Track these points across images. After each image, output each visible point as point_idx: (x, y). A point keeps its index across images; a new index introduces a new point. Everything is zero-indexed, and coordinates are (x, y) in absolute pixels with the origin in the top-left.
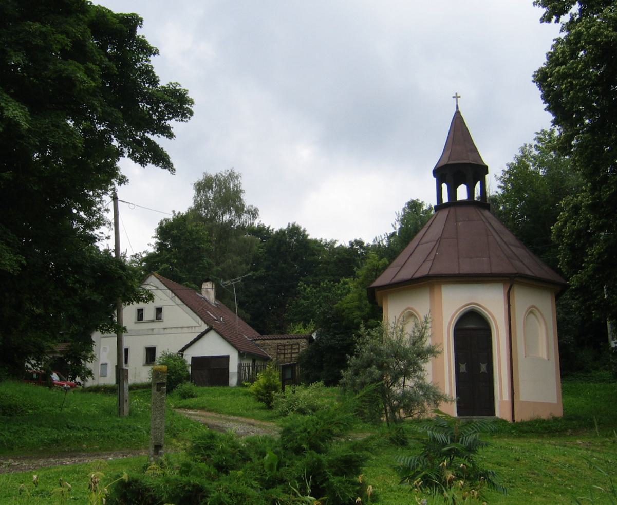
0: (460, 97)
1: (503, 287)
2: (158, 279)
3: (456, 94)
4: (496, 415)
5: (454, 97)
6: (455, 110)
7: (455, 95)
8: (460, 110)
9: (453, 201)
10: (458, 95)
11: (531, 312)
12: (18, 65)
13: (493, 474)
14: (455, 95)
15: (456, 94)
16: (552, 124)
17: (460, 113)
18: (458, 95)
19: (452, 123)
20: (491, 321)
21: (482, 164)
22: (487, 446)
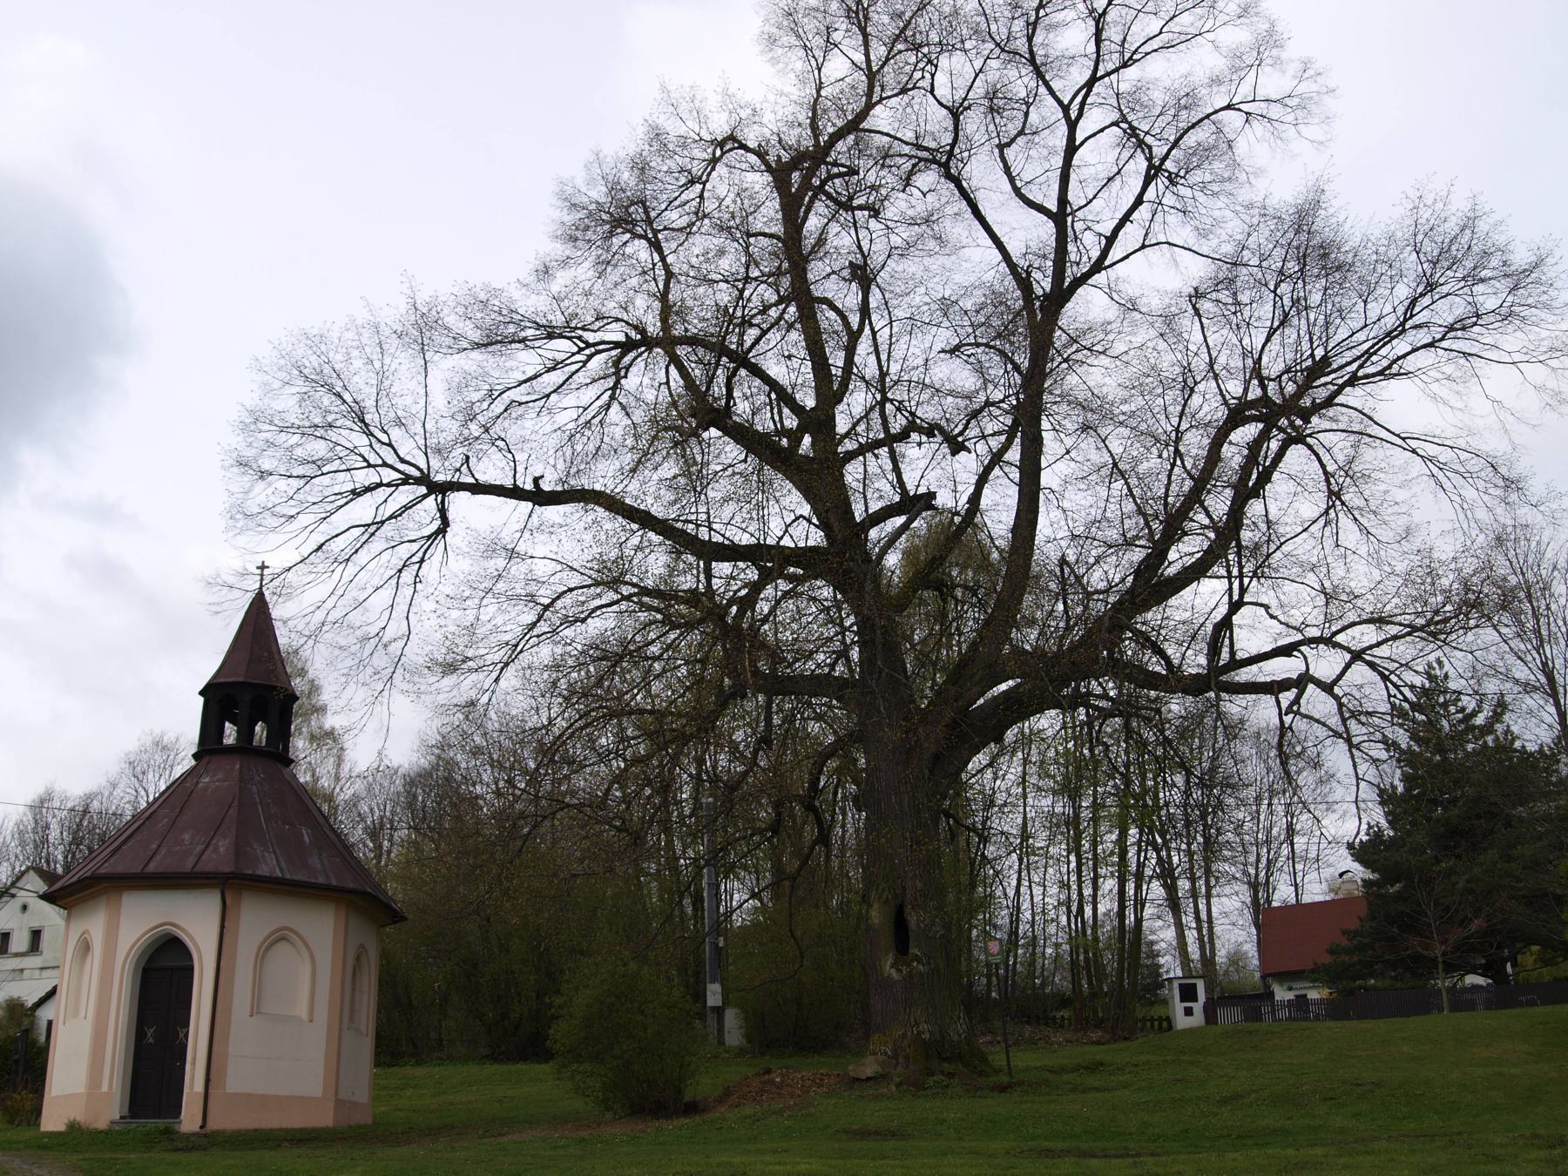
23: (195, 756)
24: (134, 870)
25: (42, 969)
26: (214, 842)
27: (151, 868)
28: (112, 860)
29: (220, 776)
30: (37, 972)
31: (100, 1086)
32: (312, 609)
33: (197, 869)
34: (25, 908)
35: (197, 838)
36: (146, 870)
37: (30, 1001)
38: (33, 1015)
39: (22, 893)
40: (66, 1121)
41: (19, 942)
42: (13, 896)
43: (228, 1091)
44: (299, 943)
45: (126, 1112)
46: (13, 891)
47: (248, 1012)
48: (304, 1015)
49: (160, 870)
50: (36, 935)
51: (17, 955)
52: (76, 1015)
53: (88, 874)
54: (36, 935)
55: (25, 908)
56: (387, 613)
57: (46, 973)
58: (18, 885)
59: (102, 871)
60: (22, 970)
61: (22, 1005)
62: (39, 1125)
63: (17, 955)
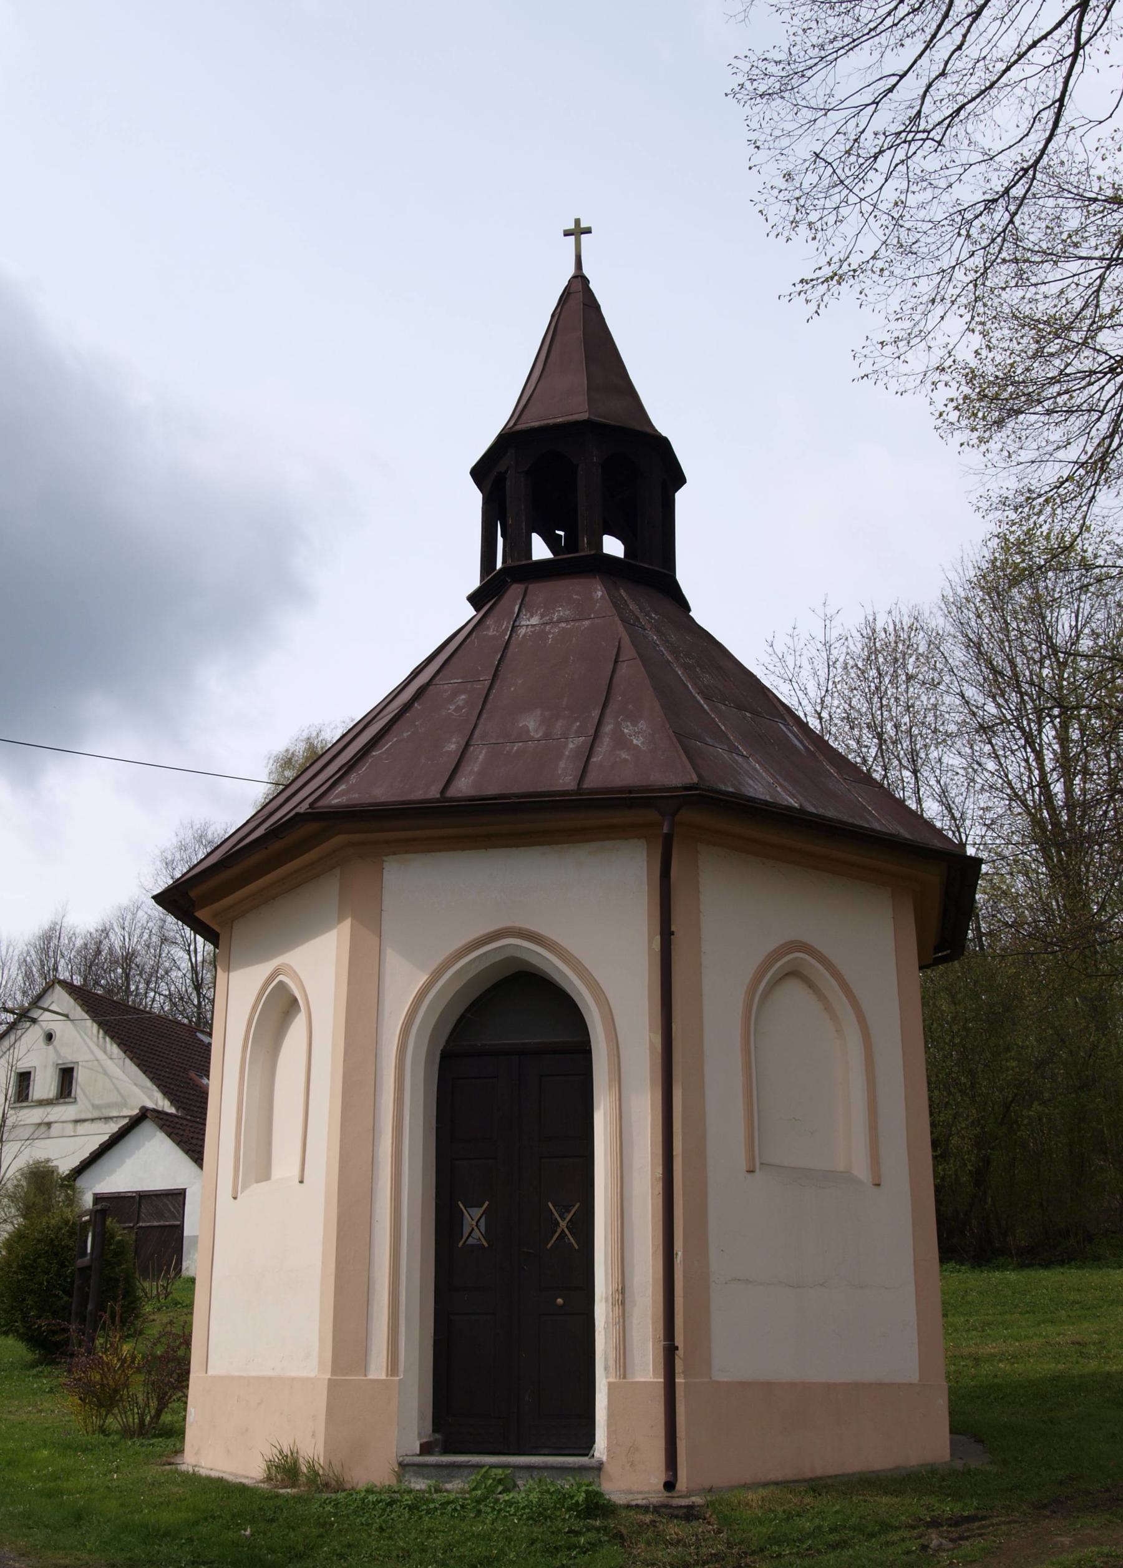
0: (588, 231)
1: (645, 857)
2: (836, 1476)
3: (577, 222)
4: (597, 1454)
5: (567, 233)
6: (571, 271)
7: (572, 226)
8: (587, 271)
9: (524, 562)
10: (583, 225)
11: (793, 973)
12: (808, 1504)
13: (831, 95)
14: (572, 226)
15: (577, 222)
16: (286, 1451)
17: (585, 281)
18: (583, 225)
19: (553, 316)
20: (583, 999)
21: (649, 430)
22: (126, 1527)
23: (475, 599)
24: (418, 795)
25: (76, 1121)
26: (608, 728)
27: (464, 786)
28: (353, 778)
29: (561, 612)
30: (70, 1126)
31: (363, 1363)
32: (867, 97)
33: (593, 781)
34: (49, 1037)
35: (560, 724)
36: (452, 792)
37: (65, 1166)
38: (72, 1187)
39: (47, 1015)
40: (271, 1453)
41: (44, 1085)
42: (34, 1021)
43: (718, 1376)
44: (831, 986)
45: (428, 1434)
46: (35, 1013)
47: (744, 1168)
48: (861, 1171)
49: (492, 790)
50: (67, 1075)
51: (42, 1103)
52: (264, 1173)
53: (302, 809)
54: (67, 1075)
55: (49, 1037)
56: (1048, 116)
57: (82, 1128)
58: (40, 1004)
59: (335, 799)
60: (49, 1125)
61: (52, 1171)
62: (176, 1433)
63: (42, 1103)
